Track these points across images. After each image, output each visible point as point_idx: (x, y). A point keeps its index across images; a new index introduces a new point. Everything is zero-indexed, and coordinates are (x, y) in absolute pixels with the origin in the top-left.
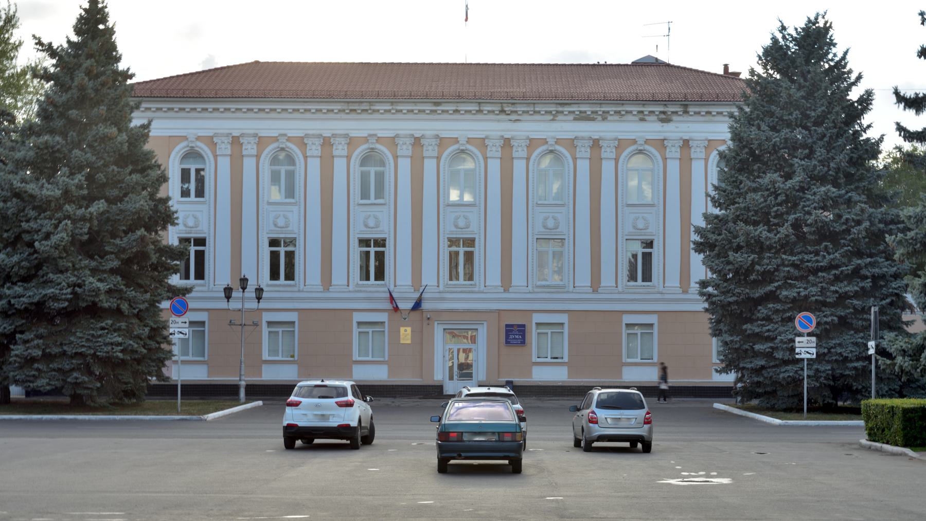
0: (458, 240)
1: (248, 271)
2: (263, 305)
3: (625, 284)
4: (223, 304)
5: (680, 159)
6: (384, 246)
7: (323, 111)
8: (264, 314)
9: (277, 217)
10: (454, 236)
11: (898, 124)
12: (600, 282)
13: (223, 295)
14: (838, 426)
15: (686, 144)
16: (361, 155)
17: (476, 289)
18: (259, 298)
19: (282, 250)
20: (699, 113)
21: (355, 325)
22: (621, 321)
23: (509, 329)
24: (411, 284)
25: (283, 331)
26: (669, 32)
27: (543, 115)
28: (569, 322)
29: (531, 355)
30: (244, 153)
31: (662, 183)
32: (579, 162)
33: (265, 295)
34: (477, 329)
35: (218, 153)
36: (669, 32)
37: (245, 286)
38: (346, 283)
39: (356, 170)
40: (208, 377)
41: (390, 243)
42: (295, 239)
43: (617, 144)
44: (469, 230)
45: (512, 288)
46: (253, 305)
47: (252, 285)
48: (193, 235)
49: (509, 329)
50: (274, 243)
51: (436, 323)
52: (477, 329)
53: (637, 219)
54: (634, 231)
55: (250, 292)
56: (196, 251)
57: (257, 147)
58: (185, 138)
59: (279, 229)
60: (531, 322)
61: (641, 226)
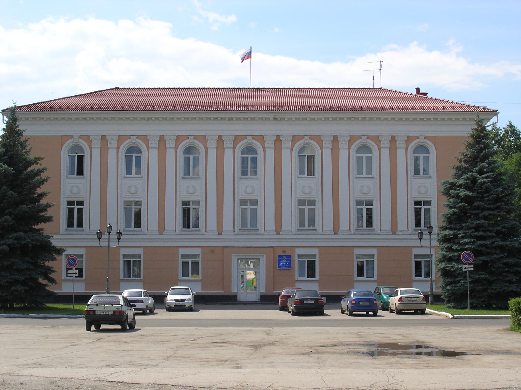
0: (305, 201)
1: (111, 220)
2: (121, 244)
3: (355, 229)
4: (96, 243)
5: (100, 148)
6: (83, 205)
7: (73, 119)
8: (180, 249)
9: (130, 187)
10: (245, 199)
11: (510, 123)
12: (397, 228)
13: (96, 237)
14: (373, 320)
15: (336, 139)
16: (242, 147)
17: (200, 233)
18: (119, 239)
19: (423, 207)
20: (28, 119)
21: (180, 257)
22: (353, 253)
23: (280, 258)
24: (333, 230)
25: (424, 260)
26: (381, 67)
27: (31, 120)
28: (144, 254)
29: (295, 276)
30: (340, 147)
31: (350, 163)
32: (209, 150)
33: (123, 237)
34: (259, 259)
35: (150, 147)
36: (381, 67)
37: (110, 231)
38: (174, 229)
39: (181, 156)
40: (85, 290)
41: (86, 203)
42: (141, 201)
43: (349, 139)
44: (137, 194)
45: (282, 232)
46: (114, 244)
47: (114, 231)
48: (76, 199)
49: (280, 258)
50: (185, 203)
51: (233, 255)
52: (259, 259)
53: (363, 187)
54: (71, 195)
55: (114, 236)
56: (309, 209)
57: (117, 142)
58: (72, 137)
59: (74, 195)
60: (294, 254)
61: (191, 191)
